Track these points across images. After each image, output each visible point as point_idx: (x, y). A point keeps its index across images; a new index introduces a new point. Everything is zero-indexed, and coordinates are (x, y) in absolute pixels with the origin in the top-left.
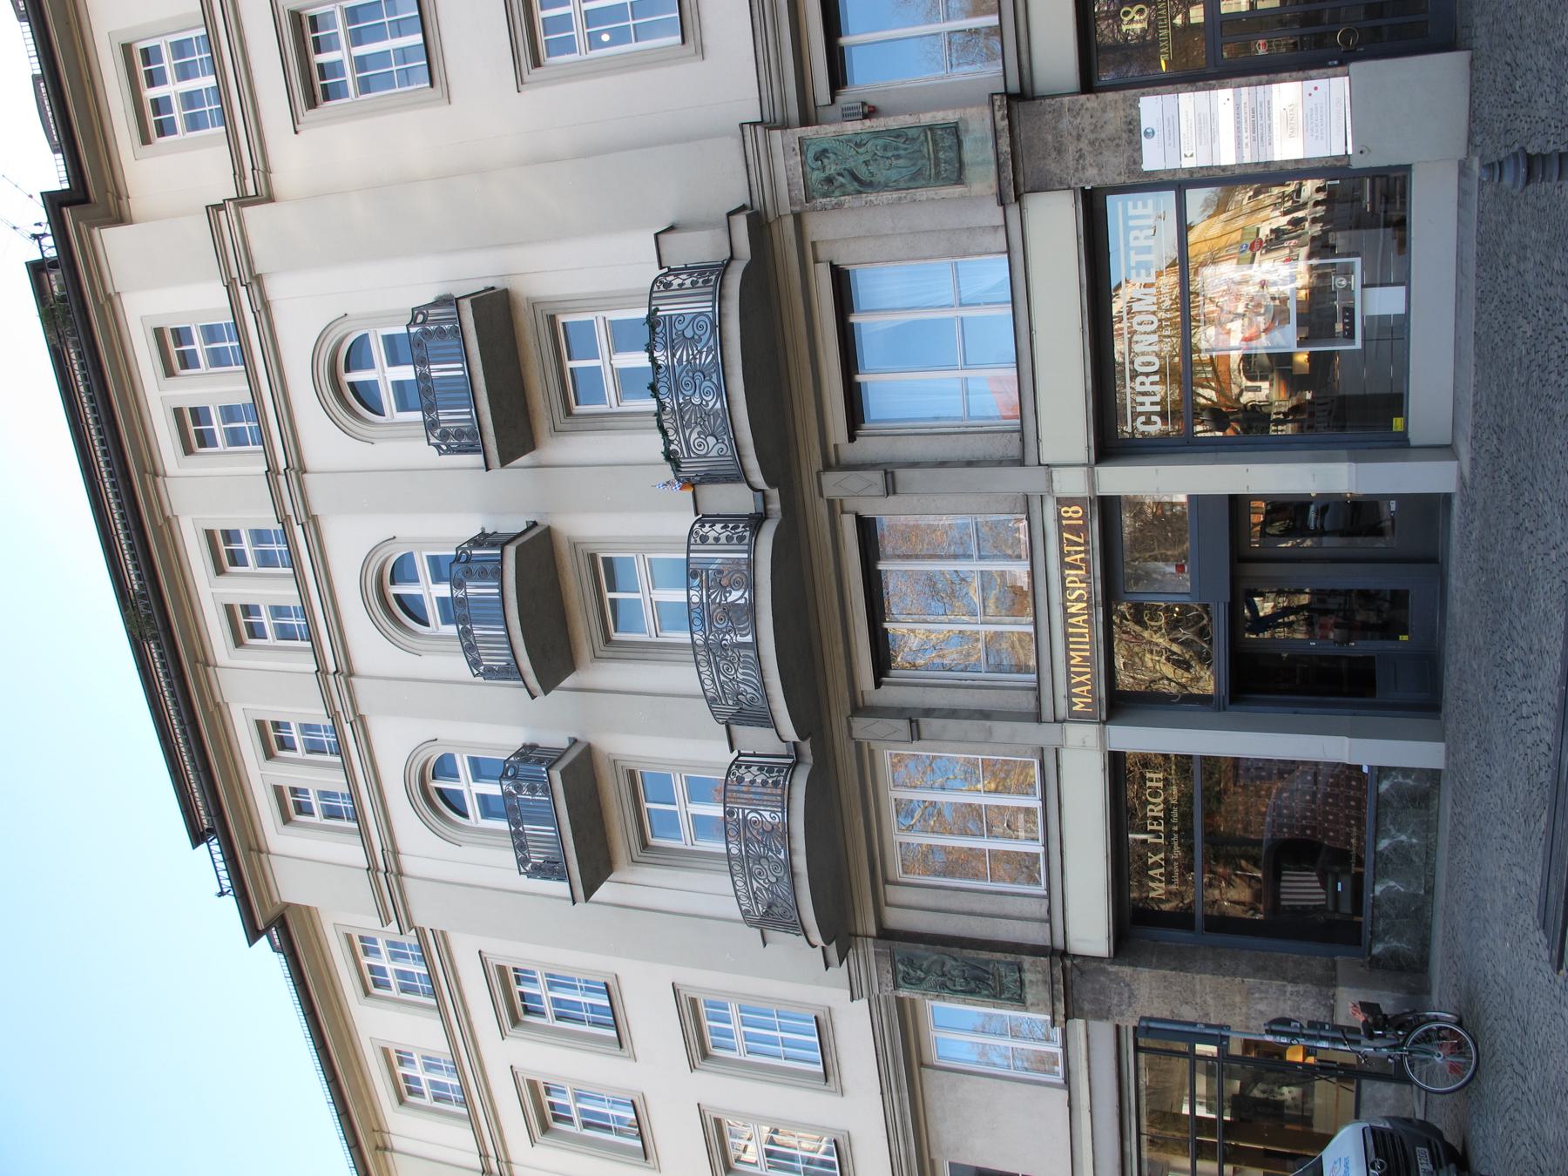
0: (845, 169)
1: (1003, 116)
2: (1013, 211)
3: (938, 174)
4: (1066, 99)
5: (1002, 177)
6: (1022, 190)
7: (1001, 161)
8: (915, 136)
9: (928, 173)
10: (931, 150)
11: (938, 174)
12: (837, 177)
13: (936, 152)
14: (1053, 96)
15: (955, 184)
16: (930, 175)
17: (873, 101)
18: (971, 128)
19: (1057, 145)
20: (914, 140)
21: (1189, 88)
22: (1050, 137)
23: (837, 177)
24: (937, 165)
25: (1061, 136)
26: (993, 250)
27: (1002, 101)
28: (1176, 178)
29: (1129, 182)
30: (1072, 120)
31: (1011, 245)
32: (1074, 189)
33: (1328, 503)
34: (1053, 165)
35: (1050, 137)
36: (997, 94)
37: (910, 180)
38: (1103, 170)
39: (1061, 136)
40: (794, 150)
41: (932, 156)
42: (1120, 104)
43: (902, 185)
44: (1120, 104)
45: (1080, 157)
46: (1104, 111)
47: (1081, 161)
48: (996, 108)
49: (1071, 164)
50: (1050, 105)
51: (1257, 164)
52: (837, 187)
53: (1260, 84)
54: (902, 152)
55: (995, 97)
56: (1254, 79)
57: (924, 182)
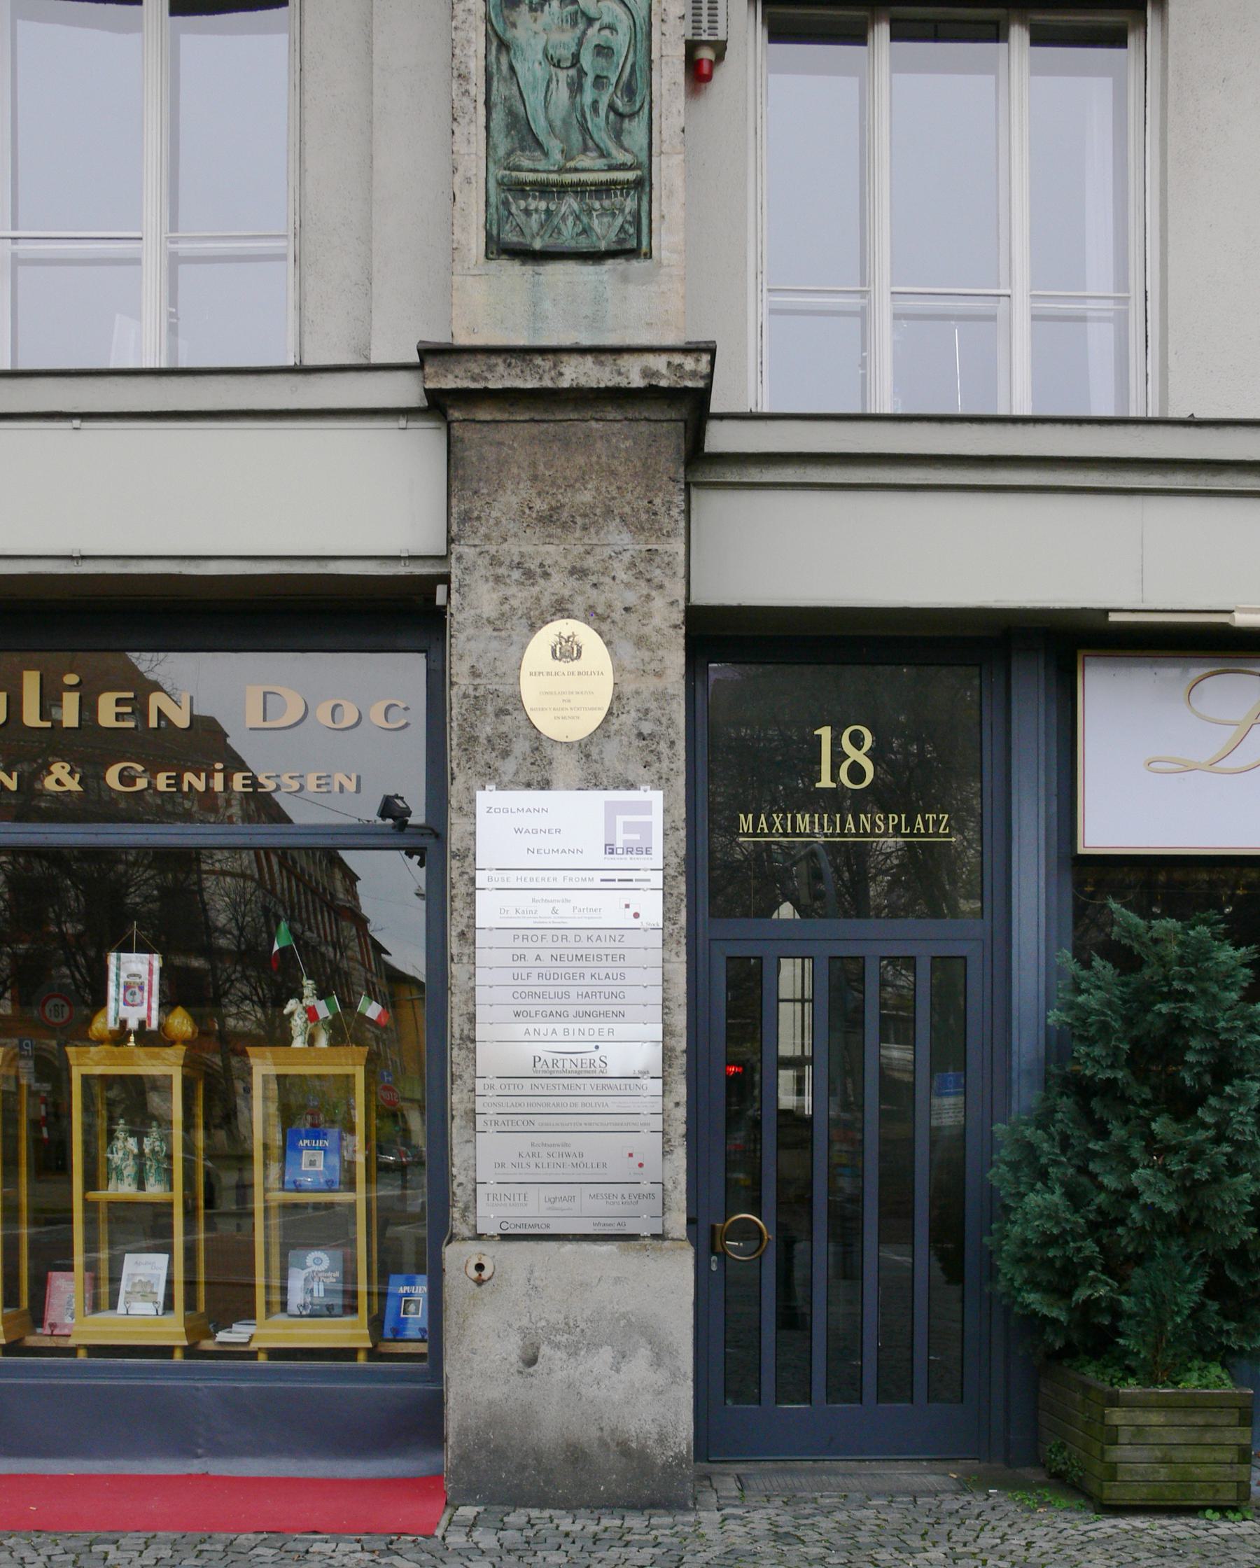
1: (656, 374)
2: (405, 390)
3: (520, 189)
4: (678, 546)
5: (494, 360)
6: (455, 414)
7: (538, 360)
8: (626, 140)
9: (526, 163)
10: (584, 177)
11: (520, 189)
13: (579, 189)
14: (687, 513)
15: (489, 236)
16: (518, 169)
17: (724, 77)
19: (565, 515)
20: (618, 135)
21: (674, 861)
22: (586, 497)
24: (544, 189)
25: (585, 528)
26: (307, 339)
27: (694, 374)
28: (453, 817)
29: (454, 695)
30: (626, 557)
31: (313, 379)
32: (449, 552)
34: (514, 500)
35: (586, 497)
36: (712, 363)
37: (511, 113)
38: (489, 631)
39: (585, 528)
41: (569, 178)
42: (651, 684)
43: (501, 90)
44: (651, 684)
45: (529, 574)
46: (640, 641)
47: (516, 574)
48: (677, 359)
49: (513, 549)
50: (669, 505)
51: (472, 1018)
53: (666, 1033)
54: (588, 96)
55: (706, 358)
56: (680, 1020)
57: (501, 152)
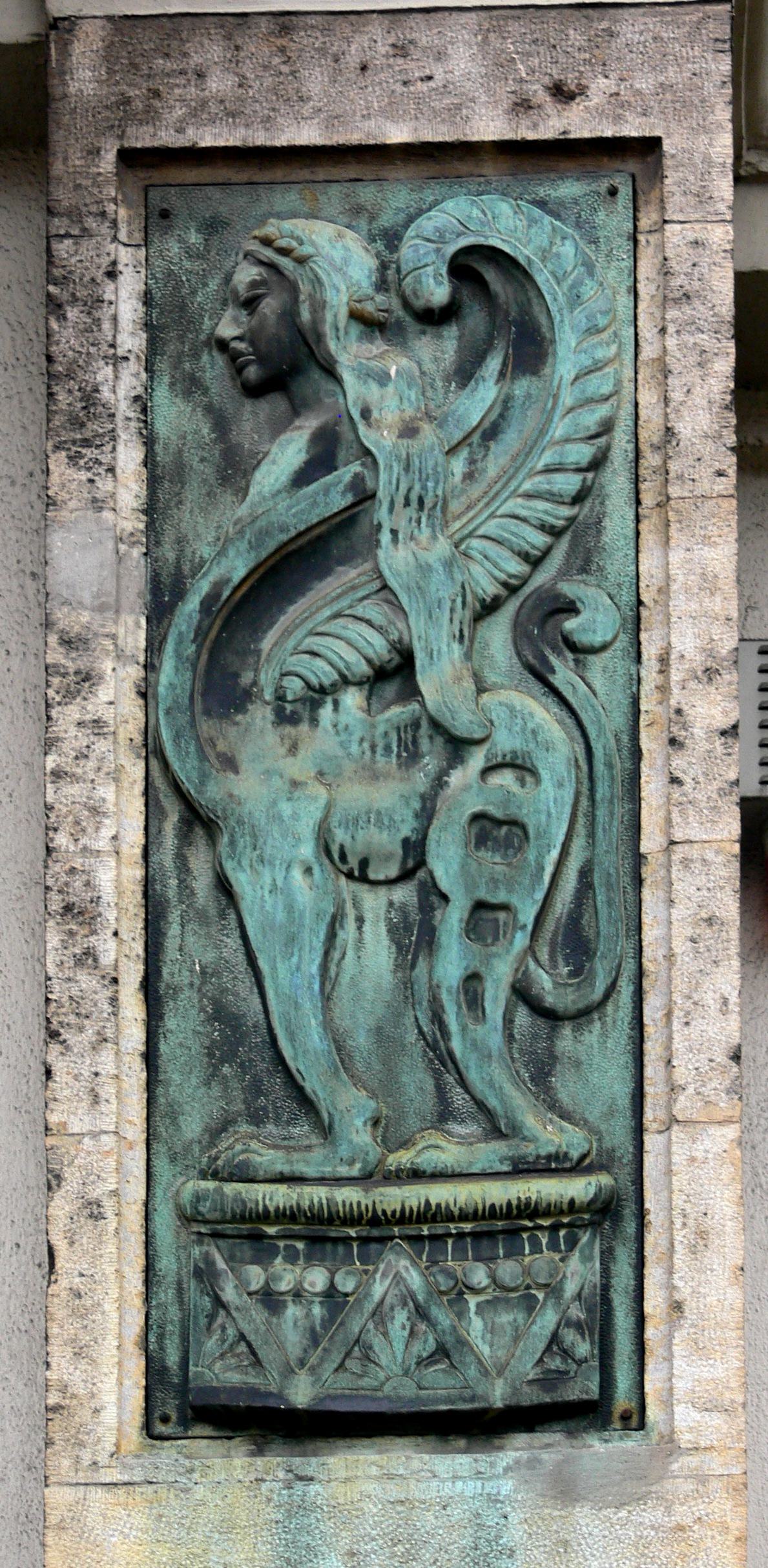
0: (364, 496)
8: (565, 1087)
9: (267, 1158)
10: (440, 1194)
12: (309, 424)
15: (154, 1372)
18: (584, 1517)
23: (309, 424)
33: (257, 581)
40: (562, 93)
41: (412, 1196)
52: (221, 424)
57: (192, 1126)
